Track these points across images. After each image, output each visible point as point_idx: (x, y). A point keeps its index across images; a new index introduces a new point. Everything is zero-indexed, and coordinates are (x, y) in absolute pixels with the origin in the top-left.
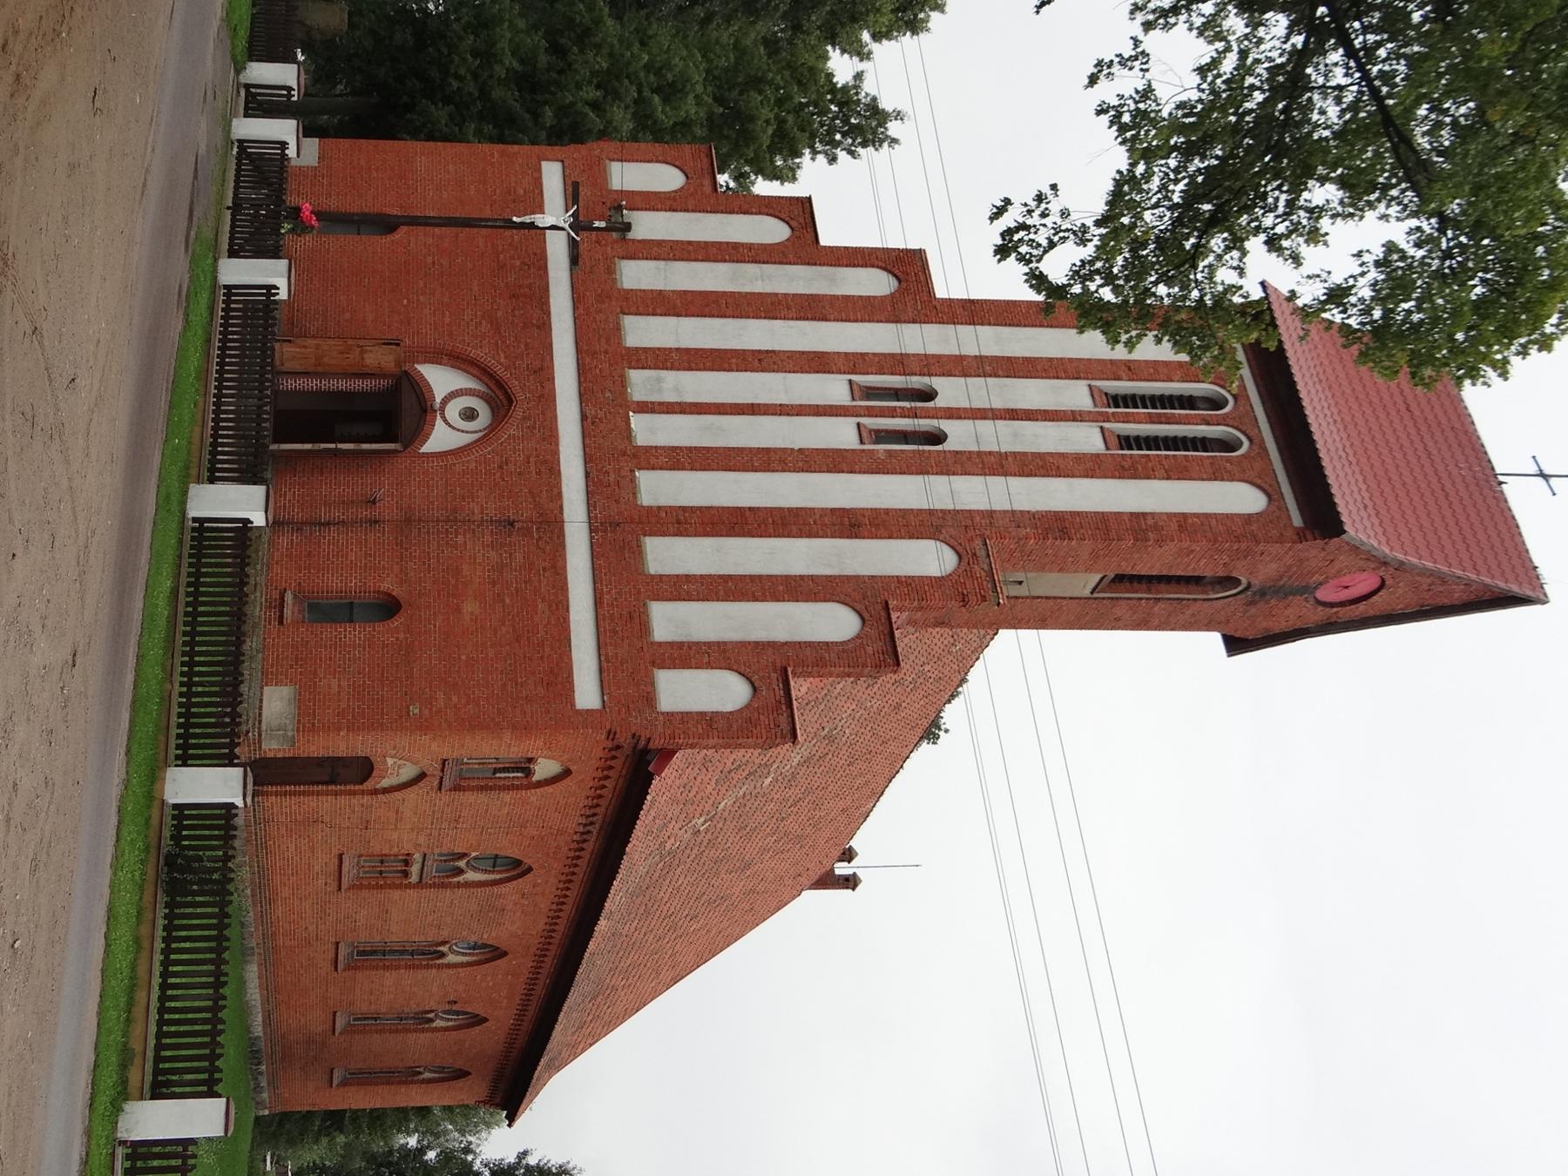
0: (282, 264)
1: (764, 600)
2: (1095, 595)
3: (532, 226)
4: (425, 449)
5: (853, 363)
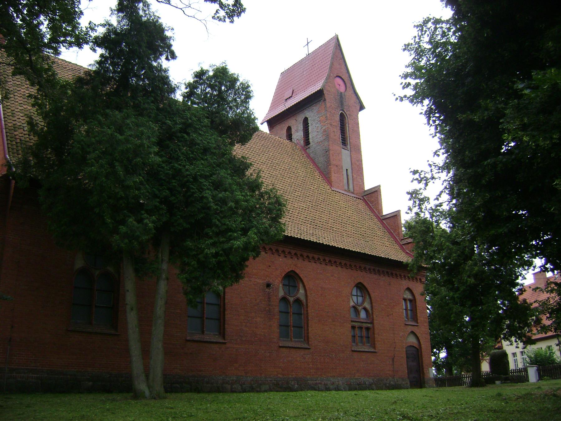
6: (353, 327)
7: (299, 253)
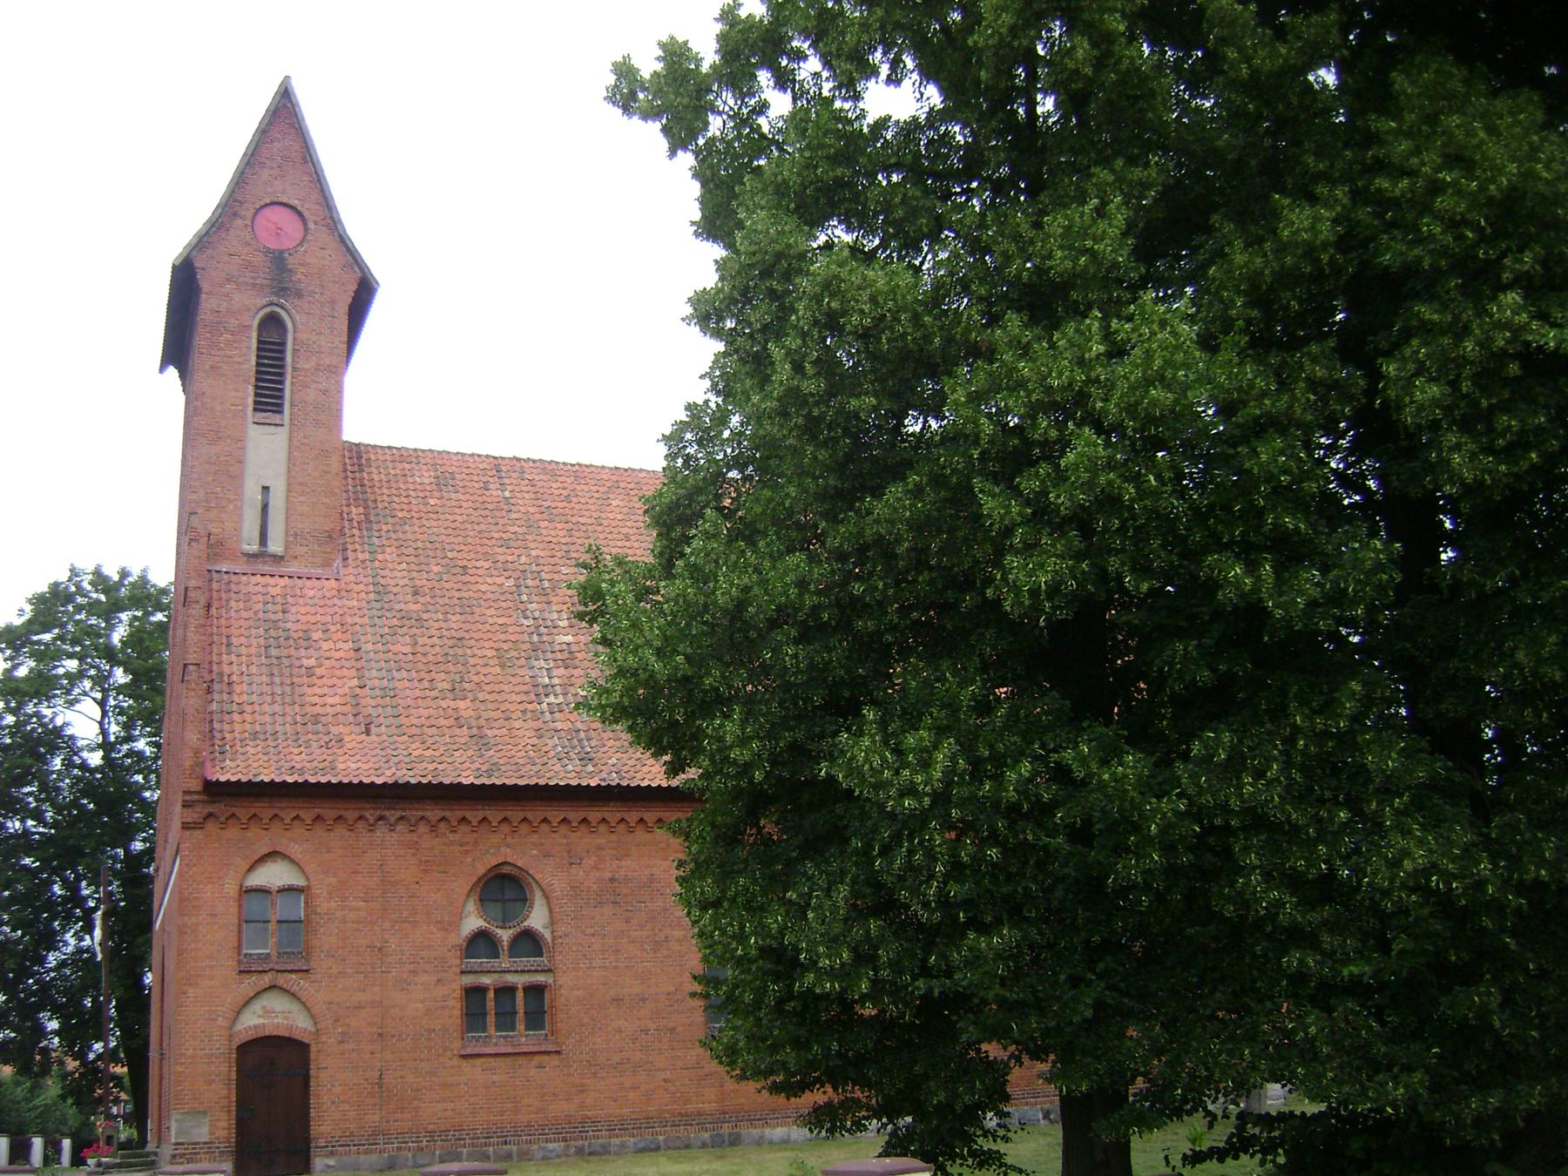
2: (287, 421)
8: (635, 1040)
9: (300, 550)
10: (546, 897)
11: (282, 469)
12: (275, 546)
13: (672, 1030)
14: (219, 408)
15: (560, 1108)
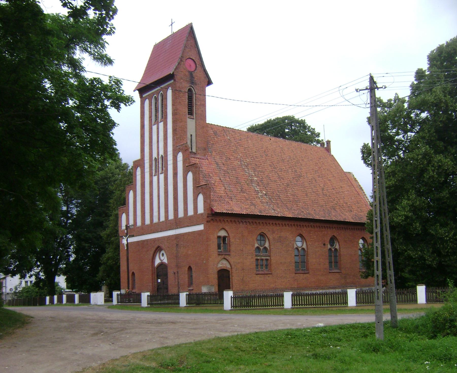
0: (142, 294)
1: (187, 192)
2: (195, 118)
3: (127, 245)
4: (167, 263)
5: (151, 176)
6: (257, 260)
7: (293, 224)
8: (284, 272)
9: (199, 152)
10: (269, 240)
11: (194, 131)
12: (194, 150)
13: (290, 270)
14: (181, 113)
15: (272, 286)
